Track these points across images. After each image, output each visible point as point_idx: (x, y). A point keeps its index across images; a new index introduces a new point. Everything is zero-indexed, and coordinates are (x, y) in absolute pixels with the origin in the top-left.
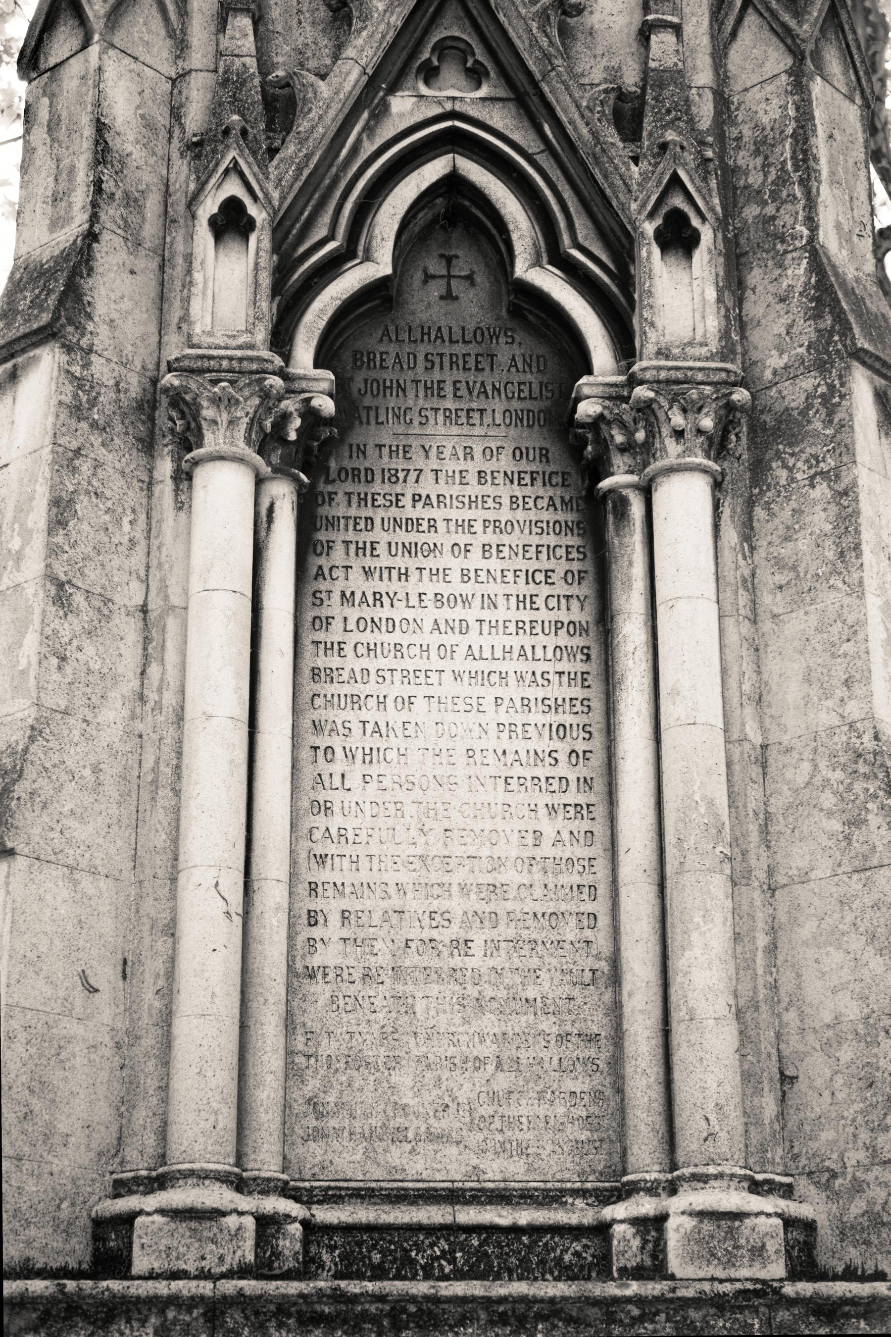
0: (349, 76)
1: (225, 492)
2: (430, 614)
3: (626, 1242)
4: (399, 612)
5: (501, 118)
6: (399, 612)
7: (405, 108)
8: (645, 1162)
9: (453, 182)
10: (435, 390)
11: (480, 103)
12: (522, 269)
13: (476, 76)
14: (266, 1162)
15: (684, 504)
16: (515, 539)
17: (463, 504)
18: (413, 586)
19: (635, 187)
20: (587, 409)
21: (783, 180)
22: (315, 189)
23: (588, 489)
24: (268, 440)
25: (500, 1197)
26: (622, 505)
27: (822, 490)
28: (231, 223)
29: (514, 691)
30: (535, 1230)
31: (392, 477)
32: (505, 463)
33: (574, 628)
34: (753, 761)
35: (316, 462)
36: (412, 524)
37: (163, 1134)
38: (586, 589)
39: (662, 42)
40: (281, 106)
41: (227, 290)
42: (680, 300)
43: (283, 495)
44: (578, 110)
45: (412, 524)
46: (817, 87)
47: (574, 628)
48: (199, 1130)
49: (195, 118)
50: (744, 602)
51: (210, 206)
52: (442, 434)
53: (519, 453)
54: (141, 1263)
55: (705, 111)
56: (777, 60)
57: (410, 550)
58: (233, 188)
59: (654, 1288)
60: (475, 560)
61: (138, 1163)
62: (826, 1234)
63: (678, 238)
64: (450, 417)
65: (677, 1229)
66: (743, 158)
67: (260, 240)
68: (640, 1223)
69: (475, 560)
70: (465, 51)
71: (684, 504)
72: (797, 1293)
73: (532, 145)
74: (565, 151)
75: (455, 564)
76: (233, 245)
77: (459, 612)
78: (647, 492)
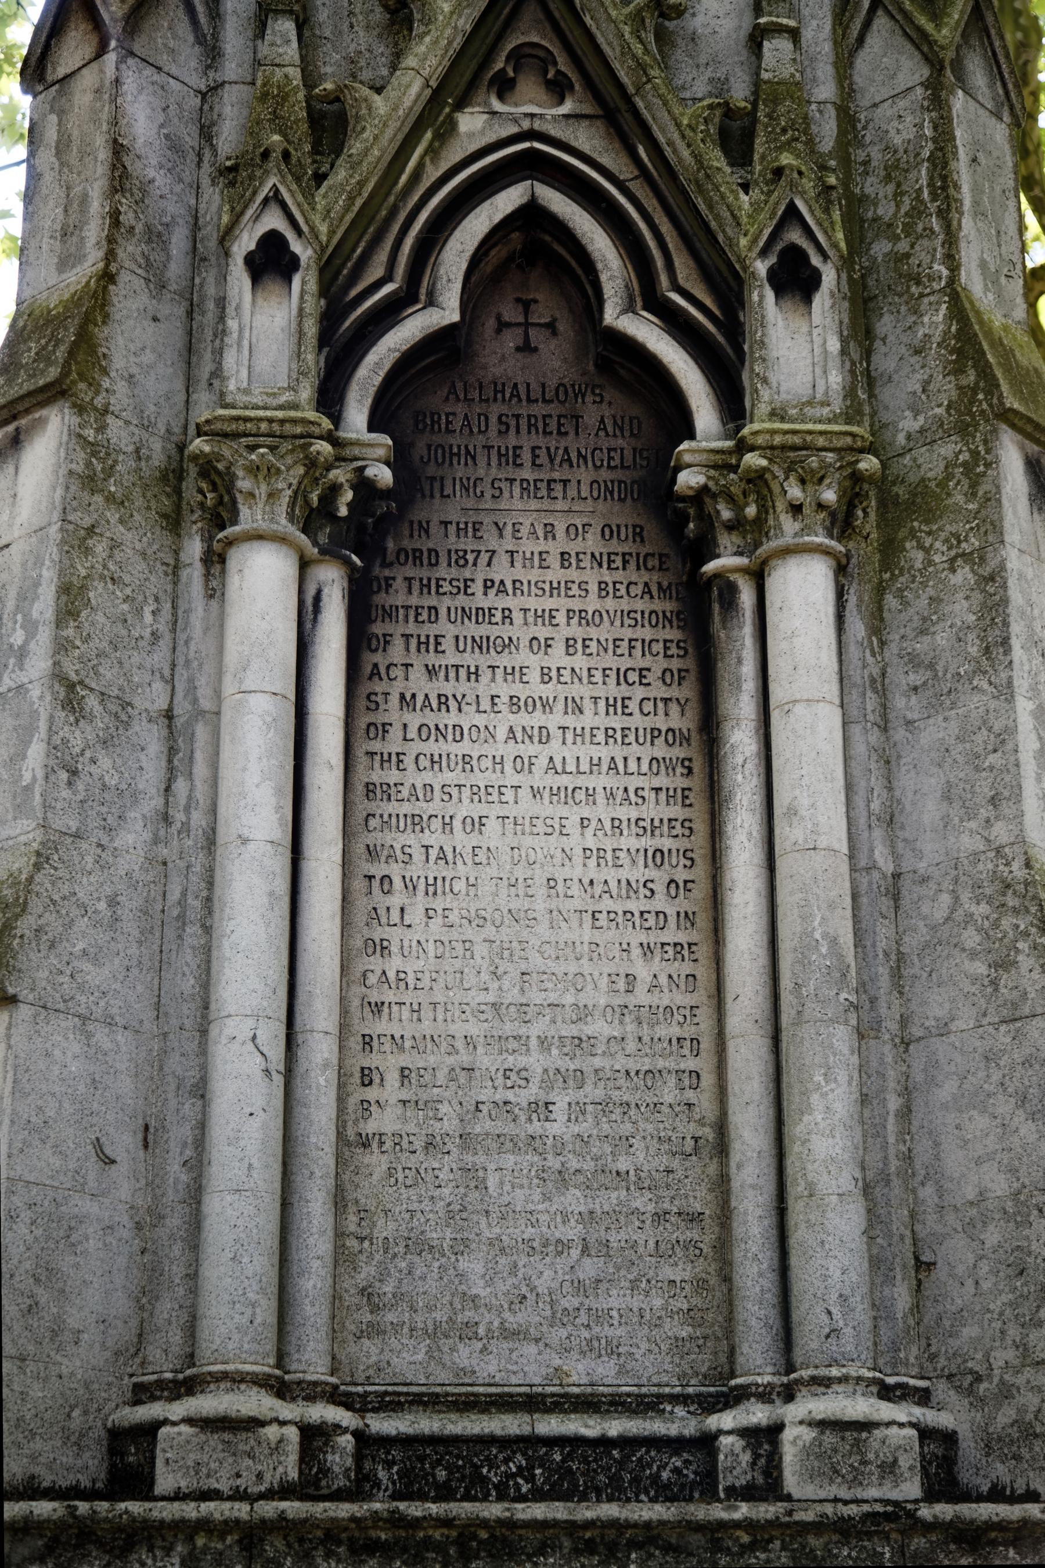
0: (410, 89)
1: (263, 578)
2: (504, 721)
3: (734, 1457)
4: (469, 718)
6: (469, 718)
7: (474, 126)
8: (757, 1362)
9: (531, 214)
10: (511, 458)
12: (612, 316)
13: (558, 89)
14: (312, 1362)
15: (803, 593)
16: (604, 632)
18: (484, 687)
19: (745, 217)
20: (689, 479)
21: (918, 211)
22: (370, 223)
24: (314, 516)
25: (587, 1404)
26: (730, 592)
27: (964, 575)
28: (271, 262)
29: (602, 811)
30: (626, 1442)
31: (460, 559)
32: (592, 543)
33: (673, 736)
34: (882, 892)
35: (375, 547)
36: (484, 615)
37: (191, 1329)
38: (687, 691)
40: (330, 125)
41: (267, 339)
42: (798, 352)
43: (332, 580)
44: (678, 126)
45: (484, 615)
46: (959, 102)
47: (673, 736)
48: (233, 1321)
49: (229, 138)
50: (871, 703)
51: (246, 242)
52: (520, 510)
53: (608, 532)
54: (165, 1481)
55: (827, 130)
56: (911, 71)
57: (481, 645)
58: (274, 221)
60: (557, 657)
61: (162, 1364)
62: (969, 1448)
63: (795, 280)
65: (795, 1440)
66: (871, 186)
67: (304, 282)
68: (749, 1434)
70: (546, 60)
71: (803, 593)
73: (624, 170)
74: (663, 178)
75: (534, 661)
76: (273, 286)
77: (538, 719)
78: (759, 577)
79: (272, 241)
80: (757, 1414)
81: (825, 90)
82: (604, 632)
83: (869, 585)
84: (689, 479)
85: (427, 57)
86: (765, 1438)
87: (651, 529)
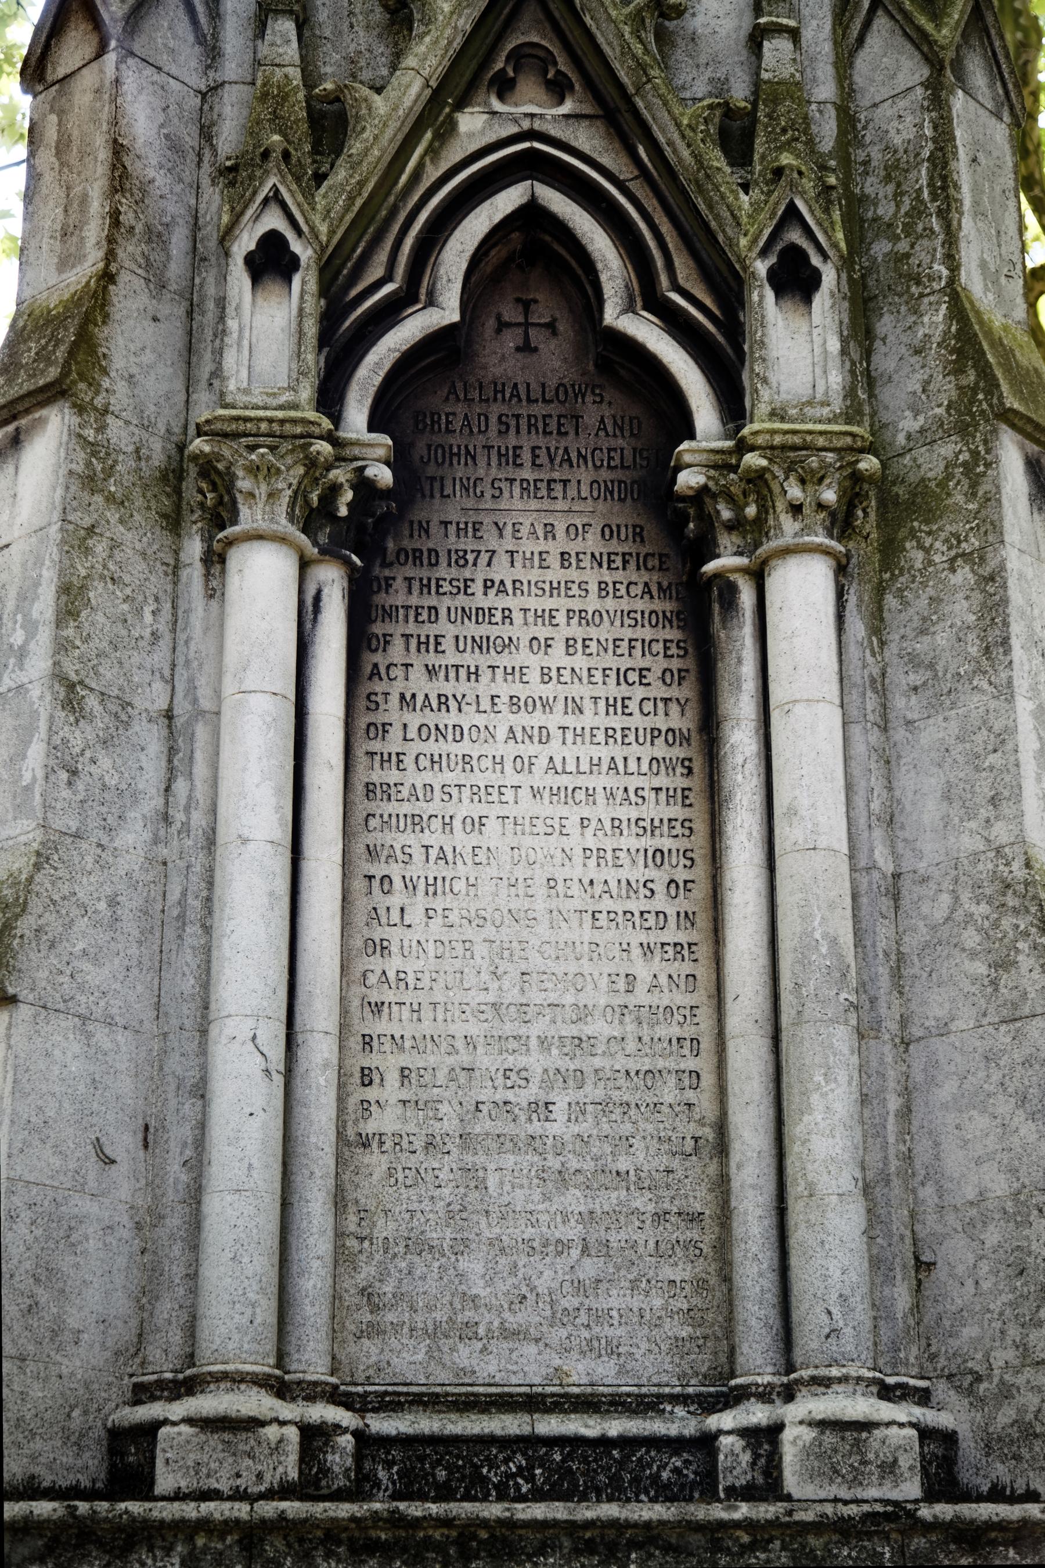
0: (410, 89)
1: (264, 578)
2: (504, 721)
4: (469, 718)
6: (469, 718)
7: (474, 126)
8: (757, 1362)
9: (532, 213)
10: (511, 458)
12: (612, 315)
13: (558, 89)
14: (312, 1362)
15: (802, 593)
16: (604, 632)
18: (484, 687)
19: (745, 217)
20: (689, 479)
21: (918, 211)
22: (370, 223)
24: (314, 516)
26: (732, 589)
27: (964, 575)
28: (271, 262)
29: (602, 811)
31: (460, 559)
32: (592, 543)
33: (673, 736)
34: (882, 892)
35: (375, 546)
36: (483, 615)
37: (191, 1329)
38: (687, 691)
40: (330, 125)
41: (267, 340)
42: (798, 353)
43: (332, 580)
44: (678, 126)
45: (483, 615)
46: (959, 102)
47: (673, 736)
48: (233, 1323)
49: (229, 138)
50: (872, 704)
51: (246, 242)
52: (520, 510)
53: (608, 532)
54: (165, 1481)
56: (911, 71)
57: (481, 645)
58: (274, 221)
60: (557, 657)
61: (162, 1364)
62: (969, 1448)
63: (795, 280)
64: (528, 489)
65: (795, 1440)
66: (872, 186)
67: (305, 281)
68: (750, 1434)
70: (546, 60)
71: (802, 593)
73: (624, 170)
74: (664, 179)
75: (534, 661)
76: (273, 287)
77: (538, 718)
78: (759, 576)
79: (272, 241)
80: (757, 1414)
81: (825, 90)
82: (604, 632)
84: (689, 479)
85: (427, 57)
86: (765, 1438)
87: (651, 530)
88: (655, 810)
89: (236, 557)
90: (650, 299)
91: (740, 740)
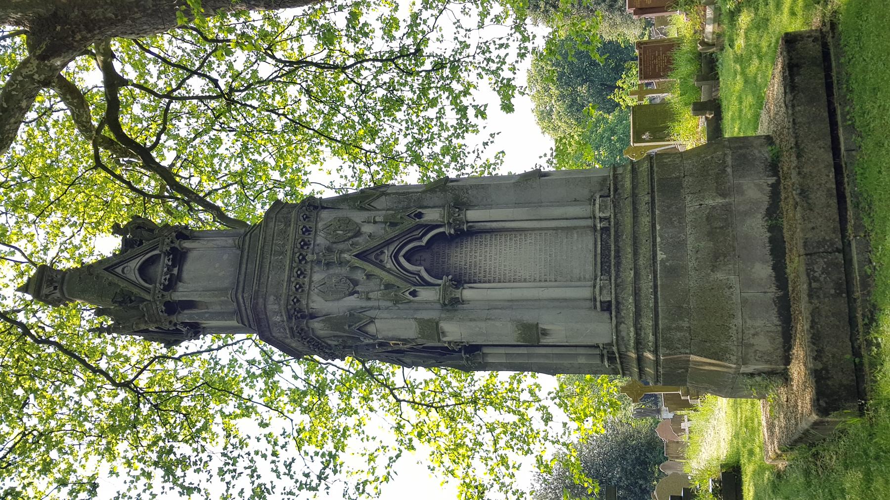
0: (383, 274)
1: (467, 293)
2: (488, 262)
3: (604, 224)
4: (488, 268)
5: (392, 248)
6: (488, 268)
7: (389, 265)
8: (589, 222)
9: (404, 256)
10: (444, 262)
11: (387, 252)
12: (423, 244)
13: (382, 252)
14: (591, 283)
15: (472, 215)
16: (474, 248)
17: (466, 256)
18: (482, 265)
19: (410, 223)
20: (452, 231)
21: (407, 198)
22: (407, 280)
23: (467, 233)
24: (457, 287)
25: (596, 248)
26: (470, 227)
27: (469, 192)
28: (414, 294)
29: (503, 247)
30: (601, 241)
31: (461, 269)
32: (458, 250)
33: (491, 237)
34: (518, 205)
35: (459, 281)
36: (470, 266)
37: (586, 299)
38: (484, 235)
39: (377, 219)
40: (388, 286)
41: (426, 294)
42: (431, 215)
43: (466, 285)
44: (392, 233)
45: (470, 266)
46: (389, 191)
47: (491, 237)
48: (586, 293)
49: (389, 304)
50: (488, 206)
51: (411, 298)
52: (453, 260)
53: (457, 247)
54: (609, 299)
55: (391, 212)
56: (383, 199)
57: (475, 266)
58: (407, 293)
59: (612, 220)
60: (478, 254)
61: (590, 304)
62: (602, 193)
63: (420, 215)
64: (449, 259)
65: (602, 215)
66: (401, 206)
67: (417, 289)
68: (601, 222)
69: (478, 254)
70: (377, 255)
71: (472, 215)
72: (689, 61)
73: (398, 242)
74: (398, 237)
75: (478, 258)
76: (418, 294)
77: (488, 257)
78: (468, 222)
79: (410, 293)
80: (598, 221)
81: (384, 212)
82: (474, 248)
83: (468, 206)
84: (452, 231)
85: (377, 271)
86: (601, 219)
87: (457, 240)
88: (503, 239)
89: (464, 298)
90: (420, 238)
91: (494, 225)
